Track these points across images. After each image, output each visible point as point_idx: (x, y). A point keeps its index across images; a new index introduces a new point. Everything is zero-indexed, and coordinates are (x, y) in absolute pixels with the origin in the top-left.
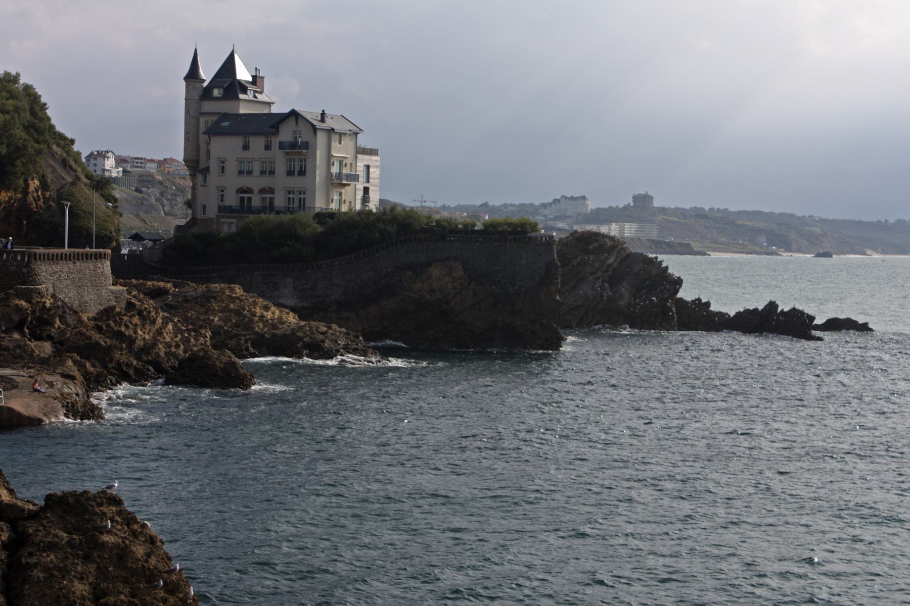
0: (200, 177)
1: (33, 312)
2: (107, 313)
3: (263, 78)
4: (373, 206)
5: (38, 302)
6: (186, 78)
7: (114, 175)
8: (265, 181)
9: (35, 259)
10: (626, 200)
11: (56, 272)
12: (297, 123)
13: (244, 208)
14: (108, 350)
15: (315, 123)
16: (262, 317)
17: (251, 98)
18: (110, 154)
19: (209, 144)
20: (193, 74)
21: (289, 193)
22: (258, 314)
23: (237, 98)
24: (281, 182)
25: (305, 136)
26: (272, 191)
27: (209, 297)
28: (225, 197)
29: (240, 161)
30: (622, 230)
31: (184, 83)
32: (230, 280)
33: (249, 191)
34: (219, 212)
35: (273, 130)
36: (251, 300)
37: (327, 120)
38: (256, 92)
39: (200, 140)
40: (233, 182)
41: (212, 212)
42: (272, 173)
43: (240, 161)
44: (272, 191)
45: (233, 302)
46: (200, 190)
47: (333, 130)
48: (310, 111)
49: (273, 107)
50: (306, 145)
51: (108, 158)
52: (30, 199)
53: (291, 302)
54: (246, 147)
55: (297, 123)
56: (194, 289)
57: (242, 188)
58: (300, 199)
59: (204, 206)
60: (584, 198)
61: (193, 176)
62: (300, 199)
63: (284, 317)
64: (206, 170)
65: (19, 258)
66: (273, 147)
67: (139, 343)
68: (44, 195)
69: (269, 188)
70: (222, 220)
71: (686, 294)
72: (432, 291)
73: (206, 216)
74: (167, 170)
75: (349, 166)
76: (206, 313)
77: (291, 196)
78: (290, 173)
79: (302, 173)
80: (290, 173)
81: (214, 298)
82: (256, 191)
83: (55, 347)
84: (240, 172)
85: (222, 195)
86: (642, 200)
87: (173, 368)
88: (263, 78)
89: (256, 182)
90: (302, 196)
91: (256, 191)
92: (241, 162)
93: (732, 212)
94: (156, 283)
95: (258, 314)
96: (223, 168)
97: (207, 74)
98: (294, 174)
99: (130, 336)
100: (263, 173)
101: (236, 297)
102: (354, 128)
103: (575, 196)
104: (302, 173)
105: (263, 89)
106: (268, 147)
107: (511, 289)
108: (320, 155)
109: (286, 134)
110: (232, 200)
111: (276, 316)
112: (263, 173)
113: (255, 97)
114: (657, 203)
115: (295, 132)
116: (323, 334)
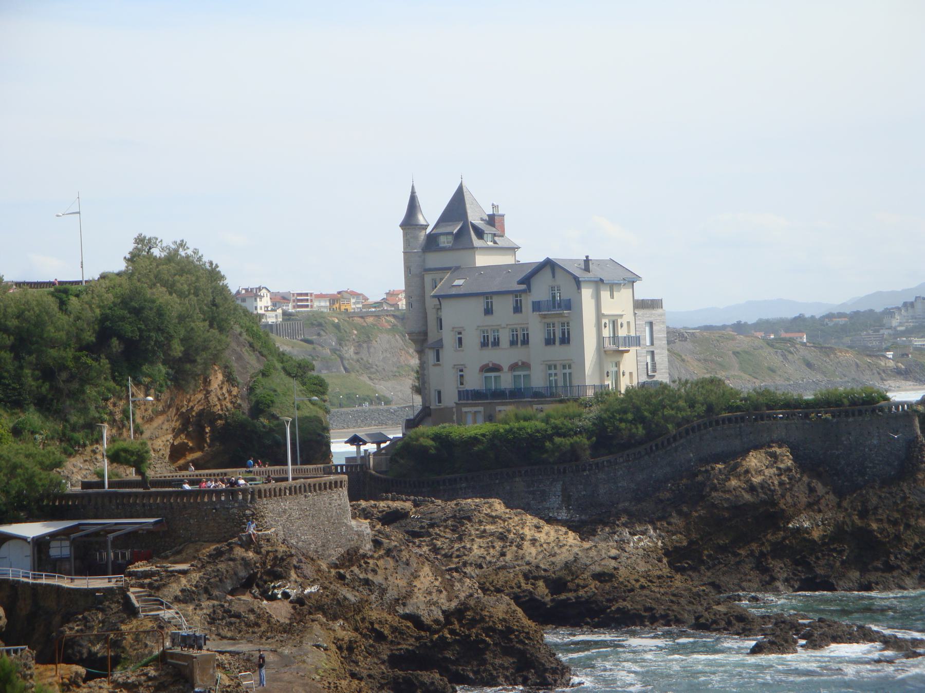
1: (264, 564)
2: (352, 557)
4: (663, 376)
5: (268, 552)
6: (402, 226)
7: (271, 320)
9: (260, 497)
11: (285, 511)
12: (554, 277)
14: (358, 608)
15: (577, 273)
16: (534, 541)
17: (491, 244)
18: (264, 292)
19: (439, 309)
20: (410, 222)
21: (550, 367)
22: (529, 537)
24: (538, 353)
25: (565, 293)
26: (526, 366)
27: (461, 518)
28: (466, 378)
31: (400, 232)
32: (486, 493)
33: (496, 368)
34: (460, 399)
35: (523, 287)
36: (516, 519)
38: (495, 235)
39: (427, 305)
40: (474, 357)
41: (450, 399)
42: (525, 342)
44: (526, 366)
45: (493, 523)
46: (433, 372)
47: (602, 280)
49: (518, 252)
50: (568, 305)
51: (261, 297)
52: (213, 399)
53: (563, 515)
54: (488, 311)
55: (554, 277)
56: (440, 507)
57: (487, 365)
58: (565, 374)
59: (439, 393)
61: (421, 352)
62: (565, 374)
63: (561, 538)
64: (438, 348)
65: (240, 497)
66: (523, 309)
67: (391, 594)
68: (230, 392)
69: (523, 363)
70: (464, 409)
72: (752, 489)
73: (442, 405)
74: (343, 308)
75: (625, 325)
76: (460, 539)
77: (553, 371)
78: (549, 342)
80: (549, 342)
81: (469, 519)
82: (506, 368)
83: (294, 608)
85: (462, 376)
87: (436, 621)
89: (504, 356)
90: (567, 371)
91: (506, 368)
94: (390, 503)
95: (529, 537)
96: (460, 340)
97: (430, 215)
98: (554, 343)
99: (381, 584)
101: (497, 517)
102: (630, 275)
104: (565, 340)
105: (503, 231)
106: (518, 309)
107: (860, 479)
109: (540, 291)
110: (474, 382)
111: (552, 538)
112: (513, 343)
113: (495, 243)
115: (553, 288)
116: (615, 558)
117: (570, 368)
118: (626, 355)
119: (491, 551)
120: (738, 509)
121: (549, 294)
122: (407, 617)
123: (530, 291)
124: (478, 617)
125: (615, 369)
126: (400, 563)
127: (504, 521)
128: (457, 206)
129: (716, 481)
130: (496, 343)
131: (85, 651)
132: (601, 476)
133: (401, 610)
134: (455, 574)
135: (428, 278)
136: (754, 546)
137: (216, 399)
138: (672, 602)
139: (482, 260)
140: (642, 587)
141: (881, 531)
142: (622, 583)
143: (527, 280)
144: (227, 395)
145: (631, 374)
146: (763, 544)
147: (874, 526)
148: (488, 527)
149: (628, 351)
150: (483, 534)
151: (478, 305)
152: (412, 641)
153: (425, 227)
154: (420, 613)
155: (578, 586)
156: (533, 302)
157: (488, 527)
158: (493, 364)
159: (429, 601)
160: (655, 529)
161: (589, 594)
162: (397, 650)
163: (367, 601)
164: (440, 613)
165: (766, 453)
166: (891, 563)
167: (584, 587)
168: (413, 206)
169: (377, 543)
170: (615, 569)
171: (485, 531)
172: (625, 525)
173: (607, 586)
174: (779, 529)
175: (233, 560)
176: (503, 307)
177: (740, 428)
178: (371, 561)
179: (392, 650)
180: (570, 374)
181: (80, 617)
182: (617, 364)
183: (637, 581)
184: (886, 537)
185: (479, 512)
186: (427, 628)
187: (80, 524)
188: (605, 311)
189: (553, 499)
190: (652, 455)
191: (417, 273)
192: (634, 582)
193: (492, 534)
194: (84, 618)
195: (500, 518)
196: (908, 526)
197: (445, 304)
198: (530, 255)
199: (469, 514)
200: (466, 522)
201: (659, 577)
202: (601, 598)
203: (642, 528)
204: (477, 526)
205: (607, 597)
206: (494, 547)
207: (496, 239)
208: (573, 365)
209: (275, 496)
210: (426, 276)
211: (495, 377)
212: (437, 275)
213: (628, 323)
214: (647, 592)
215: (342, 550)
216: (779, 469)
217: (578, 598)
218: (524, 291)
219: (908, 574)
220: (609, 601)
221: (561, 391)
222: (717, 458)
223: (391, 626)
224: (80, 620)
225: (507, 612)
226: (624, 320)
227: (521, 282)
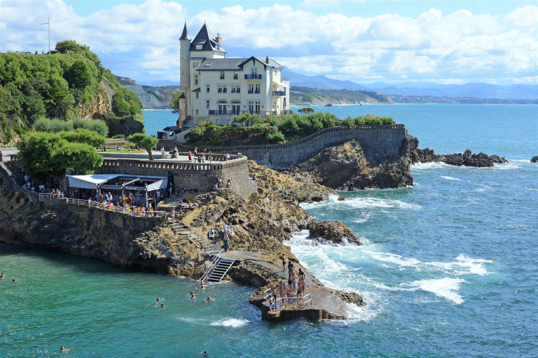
8: (236, 96)
13: (222, 111)
20: (184, 37)
21: (250, 103)
23: (211, 50)
24: (244, 98)
25: (260, 70)
40: (215, 97)
42: (239, 91)
47: (273, 67)
54: (222, 78)
58: (257, 106)
59: (197, 111)
68: (106, 105)
71: (421, 147)
72: (347, 158)
79: (257, 92)
80: (250, 92)
89: (229, 97)
97: (191, 37)
98: (252, 92)
100: (233, 91)
106: (236, 77)
110: (214, 107)
112: (233, 91)
117: (259, 103)
120: (342, 166)
127: (262, 171)
128: (204, 31)
130: (225, 91)
131: (150, 254)
132: (286, 150)
135: (192, 62)
136: (348, 182)
139: (216, 57)
141: (394, 176)
143: (241, 66)
146: (351, 181)
147: (392, 174)
160: (310, 174)
165: (351, 143)
172: (298, 172)
174: (357, 175)
175: (217, 203)
181: (144, 234)
182: (276, 103)
187: (119, 177)
189: (265, 160)
191: (186, 61)
194: (146, 235)
196: (403, 174)
212: (196, 61)
224: (144, 236)
225: (345, 231)
227: (239, 66)
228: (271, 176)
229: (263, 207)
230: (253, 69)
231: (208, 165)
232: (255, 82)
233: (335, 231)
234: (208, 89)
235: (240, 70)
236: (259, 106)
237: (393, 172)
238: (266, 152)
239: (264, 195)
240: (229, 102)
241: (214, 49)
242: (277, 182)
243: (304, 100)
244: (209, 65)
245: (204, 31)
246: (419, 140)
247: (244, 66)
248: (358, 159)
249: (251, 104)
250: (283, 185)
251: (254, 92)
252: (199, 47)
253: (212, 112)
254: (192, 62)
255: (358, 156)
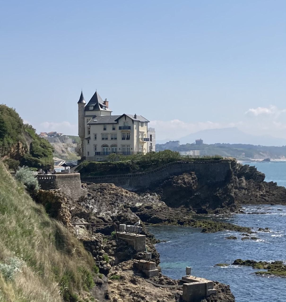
0: (86, 141)
3: (108, 102)
8: (113, 142)
9: (55, 178)
10: (194, 142)
12: (126, 119)
16: (126, 196)
21: (123, 146)
23: (99, 110)
24: (120, 142)
25: (130, 124)
26: (115, 146)
29: (102, 134)
30: (194, 153)
31: (78, 105)
33: (107, 146)
35: (116, 122)
37: (137, 117)
40: (100, 142)
41: (92, 154)
42: (116, 139)
43: (102, 134)
44: (115, 146)
48: (130, 114)
50: (129, 128)
52: (20, 151)
54: (105, 129)
55: (126, 119)
59: (88, 153)
60: (178, 141)
63: (134, 195)
72: (185, 183)
73: (89, 156)
79: (128, 138)
80: (123, 139)
81: (105, 189)
84: (103, 139)
85: (96, 148)
86: (199, 142)
88: (108, 102)
89: (109, 143)
92: (103, 135)
93: (231, 145)
96: (96, 137)
97: (86, 101)
98: (125, 139)
100: (112, 139)
101: (114, 189)
102: (147, 121)
103: (174, 141)
104: (128, 138)
106: (114, 129)
108: (135, 131)
110: (99, 150)
112: (112, 139)
113: (106, 109)
114: (204, 143)
117: (129, 146)
118: (145, 143)
119: (114, 199)
121: (125, 125)
122: (100, 218)
123: (118, 123)
124: (125, 219)
125: (141, 147)
126: (96, 201)
127: (116, 190)
128: (95, 98)
129: (175, 181)
133: (98, 216)
134: (112, 205)
135: (86, 119)
137: (21, 151)
138: (170, 215)
140: (160, 211)
141: (220, 196)
142: (154, 209)
143: (117, 120)
144: (24, 151)
145: (146, 149)
148: (112, 192)
149: (145, 142)
150: (110, 194)
151: (102, 127)
152: (103, 226)
153: (85, 104)
154: (104, 217)
155: (141, 210)
156: (119, 127)
157: (112, 192)
158: (106, 145)
159: (106, 213)
161: (145, 213)
162: (99, 228)
163: (91, 213)
164: (110, 217)
166: (223, 205)
167: (143, 211)
168: (82, 98)
169: (89, 195)
170: (152, 205)
171: (111, 193)
173: (150, 210)
176: (109, 129)
177: (182, 165)
178: (88, 200)
179: (97, 228)
180: (129, 148)
182: (142, 146)
183: (159, 209)
184: (221, 198)
185: (108, 187)
186: (107, 222)
188: (140, 130)
190: (156, 172)
192: (158, 209)
193: (113, 194)
195: (115, 189)
197: (92, 127)
198: (117, 112)
199: (105, 188)
200: (104, 190)
201: (164, 208)
202: (148, 214)
203: (154, 194)
204: (108, 191)
205: (150, 213)
206: (114, 198)
207: (106, 108)
208: (130, 147)
209: (77, 177)
210: (85, 118)
211: (106, 149)
212: (88, 118)
213: (146, 134)
214: (162, 212)
215: (80, 197)
216: (192, 178)
217: (141, 213)
218: (116, 123)
219: (227, 208)
220: (150, 215)
221: (127, 152)
222: (175, 175)
223: (97, 221)
226: (145, 133)
228: (122, 193)
229: (88, 205)
230: (124, 123)
231: (51, 176)
232: (126, 131)
233: (127, 218)
234: (96, 137)
235: (116, 123)
236: (129, 148)
237: (219, 193)
238: (128, 179)
239: (91, 197)
240: (109, 146)
241: (101, 109)
242: (124, 197)
243: (247, 155)
244: (96, 120)
245: (95, 98)
246: (265, 175)
247: (119, 120)
248: (193, 184)
249: (124, 147)
250: (128, 199)
251: (126, 139)
252: (92, 108)
253: (97, 154)
254: (86, 119)
255: (193, 182)
